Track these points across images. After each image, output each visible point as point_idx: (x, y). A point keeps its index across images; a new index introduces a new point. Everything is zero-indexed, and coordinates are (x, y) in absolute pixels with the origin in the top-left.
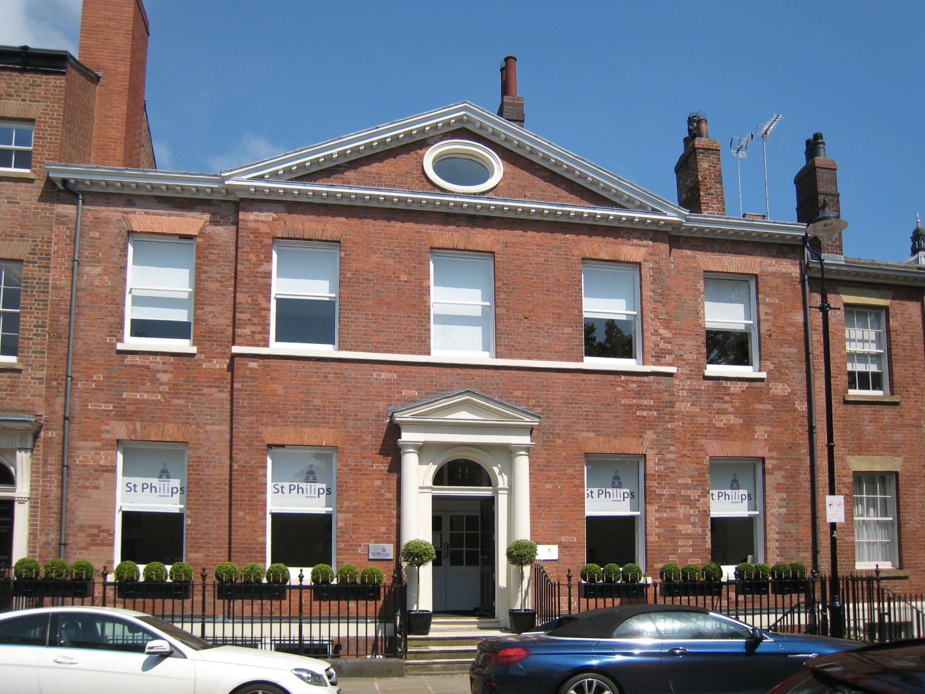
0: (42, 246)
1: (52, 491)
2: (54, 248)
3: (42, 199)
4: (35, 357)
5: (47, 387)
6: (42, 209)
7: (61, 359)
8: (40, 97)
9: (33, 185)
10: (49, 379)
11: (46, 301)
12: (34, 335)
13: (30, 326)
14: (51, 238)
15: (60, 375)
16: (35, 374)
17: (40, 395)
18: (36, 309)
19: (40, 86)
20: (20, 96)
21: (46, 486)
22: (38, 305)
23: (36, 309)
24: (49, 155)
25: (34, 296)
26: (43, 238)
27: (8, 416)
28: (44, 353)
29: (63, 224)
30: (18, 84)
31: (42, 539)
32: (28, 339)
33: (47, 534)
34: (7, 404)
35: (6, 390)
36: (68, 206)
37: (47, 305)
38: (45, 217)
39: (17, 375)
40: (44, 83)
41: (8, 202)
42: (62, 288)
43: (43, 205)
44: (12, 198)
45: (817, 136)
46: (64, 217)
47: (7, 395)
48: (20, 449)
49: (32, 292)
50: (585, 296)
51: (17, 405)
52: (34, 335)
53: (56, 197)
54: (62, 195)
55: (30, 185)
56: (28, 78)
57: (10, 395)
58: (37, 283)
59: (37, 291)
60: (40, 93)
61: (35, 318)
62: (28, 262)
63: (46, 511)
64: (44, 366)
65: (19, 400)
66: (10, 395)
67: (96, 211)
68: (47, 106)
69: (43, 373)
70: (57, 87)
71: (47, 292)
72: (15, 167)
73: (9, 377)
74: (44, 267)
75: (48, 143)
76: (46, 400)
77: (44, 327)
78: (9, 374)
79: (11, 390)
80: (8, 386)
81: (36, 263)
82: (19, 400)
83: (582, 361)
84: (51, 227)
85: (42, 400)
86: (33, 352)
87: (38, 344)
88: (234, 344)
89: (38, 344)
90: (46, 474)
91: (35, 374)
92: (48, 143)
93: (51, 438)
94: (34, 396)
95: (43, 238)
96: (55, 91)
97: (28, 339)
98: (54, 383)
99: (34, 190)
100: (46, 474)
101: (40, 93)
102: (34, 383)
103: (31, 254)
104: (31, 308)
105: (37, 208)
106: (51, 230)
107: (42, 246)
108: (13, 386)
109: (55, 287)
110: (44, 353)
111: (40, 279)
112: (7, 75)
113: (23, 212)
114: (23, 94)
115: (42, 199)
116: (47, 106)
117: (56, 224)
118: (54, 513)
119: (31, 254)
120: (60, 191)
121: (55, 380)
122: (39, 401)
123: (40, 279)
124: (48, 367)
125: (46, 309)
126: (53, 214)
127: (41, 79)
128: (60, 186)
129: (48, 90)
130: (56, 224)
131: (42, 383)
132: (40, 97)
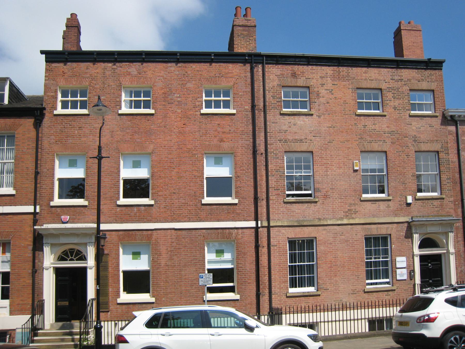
0: (445, 144)
1: (461, 249)
2: (449, 145)
3: (442, 124)
4: (448, 192)
5: (454, 205)
6: (443, 128)
7: (458, 192)
8: (434, 80)
9: (438, 118)
10: (455, 201)
11: (450, 168)
12: (447, 183)
13: (445, 179)
14: (448, 141)
15: (458, 199)
16: (449, 199)
17: (452, 208)
18: (446, 172)
19: (433, 75)
20: (427, 80)
21: (458, 247)
22: (447, 170)
23: (446, 172)
24: (442, 105)
25: (445, 166)
26: (445, 141)
27: (427, 219)
28: (451, 190)
29: (451, 134)
30: (425, 75)
31: (459, 269)
32: (445, 185)
33: (461, 267)
34: (440, 213)
35: (439, 207)
36: (452, 127)
37: (450, 170)
38: (444, 132)
39: (443, 200)
40: (435, 74)
41: (430, 126)
42: (454, 162)
43: (442, 127)
44: (430, 124)
45: (74, 16)
46: (451, 131)
47: (440, 209)
48: (450, 232)
49: (444, 164)
50: (207, 166)
51: (444, 213)
52: (447, 183)
53: (447, 123)
54: (449, 122)
55: (436, 119)
56: (428, 72)
57: (441, 209)
58: (445, 161)
59: (446, 164)
60: (434, 78)
61: (446, 175)
62: (441, 152)
63: (460, 257)
64: (452, 196)
65: (444, 211)
66: (441, 209)
67: (463, 128)
68: (437, 84)
69: (452, 199)
70: (439, 75)
71: (449, 164)
72: (373, 110)
73: (440, 202)
74: (446, 154)
75: (441, 100)
76: (455, 210)
77: (450, 179)
78: (440, 200)
79: (441, 207)
80: (440, 205)
81: (444, 152)
82: (444, 211)
83: (43, 226)
84: (447, 136)
85: (453, 210)
86: (447, 190)
87: (449, 187)
88: (35, 214)
89: (449, 187)
90: (458, 242)
91: (449, 199)
92: (441, 100)
93: (458, 226)
94: (450, 209)
95: (445, 141)
96: (439, 77)
97: (445, 185)
98: (457, 203)
99: (438, 120)
100: (458, 242)
101: (434, 78)
102: (449, 203)
103: (441, 148)
104: (444, 172)
105: (441, 128)
106: (447, 137)
107: (445, 144)
108: (442, 205)
109: (452, 162)
110: (451, 190)
111: (446, 159)
112: (420, 71)
113: (436, 130)
114: (428, 79)
115: (442, 124)
116: (437, 84)
117: (449, 134)
118: (463, 258)
119: (441, 148)
120: (448, 120)
121: (457, 201)
122: (452, 211)
123: (446, 159)
124: (454, 196)
125: (450, 172)
126: (447, 130)
127: (433, 72)
128: (449, 118)
129: (437, 77)
130: (449, 134)
131: (452, 203)
132: (434, 80)
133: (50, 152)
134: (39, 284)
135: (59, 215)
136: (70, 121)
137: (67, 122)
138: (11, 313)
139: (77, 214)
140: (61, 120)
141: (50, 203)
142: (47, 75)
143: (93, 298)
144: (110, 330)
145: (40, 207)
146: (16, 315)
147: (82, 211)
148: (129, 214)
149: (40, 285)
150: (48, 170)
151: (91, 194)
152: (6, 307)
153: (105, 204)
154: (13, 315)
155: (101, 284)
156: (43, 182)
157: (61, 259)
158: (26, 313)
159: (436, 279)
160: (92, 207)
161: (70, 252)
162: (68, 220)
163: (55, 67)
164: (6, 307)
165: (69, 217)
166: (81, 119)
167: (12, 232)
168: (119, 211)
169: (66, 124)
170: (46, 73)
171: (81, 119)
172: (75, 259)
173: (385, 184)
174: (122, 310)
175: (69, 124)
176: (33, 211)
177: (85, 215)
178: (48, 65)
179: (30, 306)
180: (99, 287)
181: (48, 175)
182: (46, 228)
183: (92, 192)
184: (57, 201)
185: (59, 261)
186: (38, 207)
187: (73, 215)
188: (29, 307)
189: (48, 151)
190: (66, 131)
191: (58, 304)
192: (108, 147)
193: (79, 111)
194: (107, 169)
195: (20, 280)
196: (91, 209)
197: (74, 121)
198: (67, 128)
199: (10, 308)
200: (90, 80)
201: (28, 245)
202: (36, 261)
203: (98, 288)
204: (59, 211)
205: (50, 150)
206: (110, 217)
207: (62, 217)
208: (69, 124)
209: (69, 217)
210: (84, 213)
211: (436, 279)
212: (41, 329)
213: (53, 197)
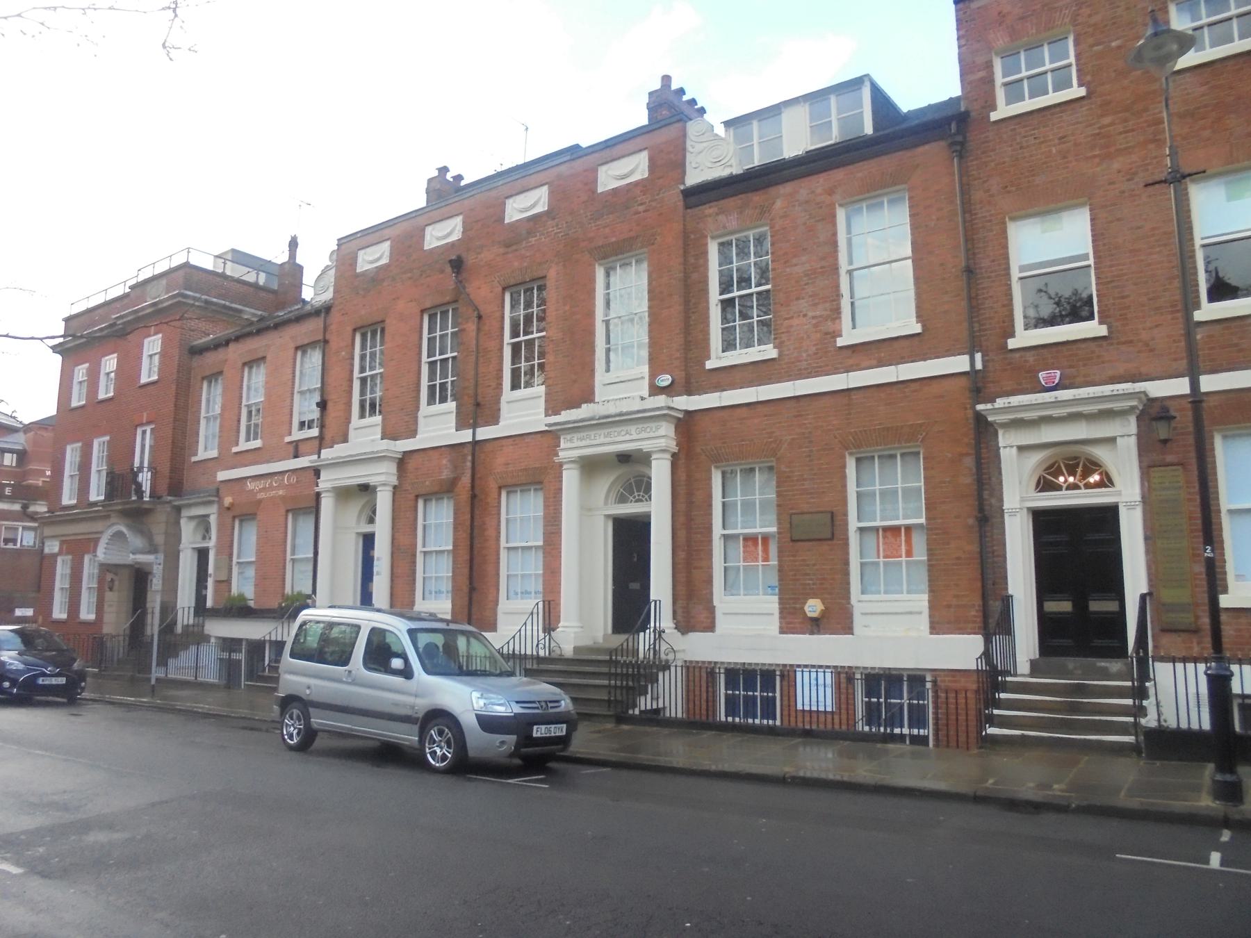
88: (972, 374)
133: (991, 215)
134: (996, 554)
135: (1033, 373)
136: (1034, 129)
137: (1026, 132)
138: (935, 628)
139: (1081, 363)
140: (1012, 130)
141: (1006, 343)
142: (962, 32)
143: (1145, 592)
144: (1192, 690)
145: (983, 356)
146: (944, 634)
147: (1093, 352)
148: (1236, 345)
149: (998, 556)
150: (993, 261)
151: (1114, 304)
152: (920, 613)
153: (1157, 326)
154: (937, 634)
155: (1215, 545)
156: (983, 294)
157: (1045, 485)
158: (969, 631)
159: (1123, 856)
160: (1123, 340)
161: (1085, 466)
162: (1057, 381)
163: (978, 8)
164: (772, 614)
165: (1058, 372)
166: (1061, 117)
167: (921, 425)
168: (1203, 338)
169: (1025, 137)
170: (958, 30)
171: (1061, 117)
172: (1081, 485)
173: (1027, 101)
174: (1240, 630)
175: (1031, 135)
176: (967, 368)
177: (1103, 363)
178: (961, 10)
179: (977, 611)
180: (1212, 551)
181: (993, 274)
182: (1007, 405)
183: (1114, 298)
184: (1024, 338)
185: (1039, 492)
186: (978, 356)
187: (1071, 367)
188: (973, 613)
189: (988, 214)
190: (1026, 155)
191: (1117, 603)
192: (1147, 170)
193: (1053, 98)
194: (1153, 229)
195: (948, 544)
196: (1118, 344)
197: (1044, 127)
198: (1028, 146)
199: (930, 616)
200: (1075, 10)
201: (962, 455)
202: (986, 494)
203: (1211, 555)
204: (1031, 359)
205: (993, 212)
206: (1175, 360)
207: (1042, 375)
208: (1031, 135)
209: (1058, 372)
210: (1099, 357)
211: (1123, 856)
212: (1008, 673)
213: (1013, 326)
